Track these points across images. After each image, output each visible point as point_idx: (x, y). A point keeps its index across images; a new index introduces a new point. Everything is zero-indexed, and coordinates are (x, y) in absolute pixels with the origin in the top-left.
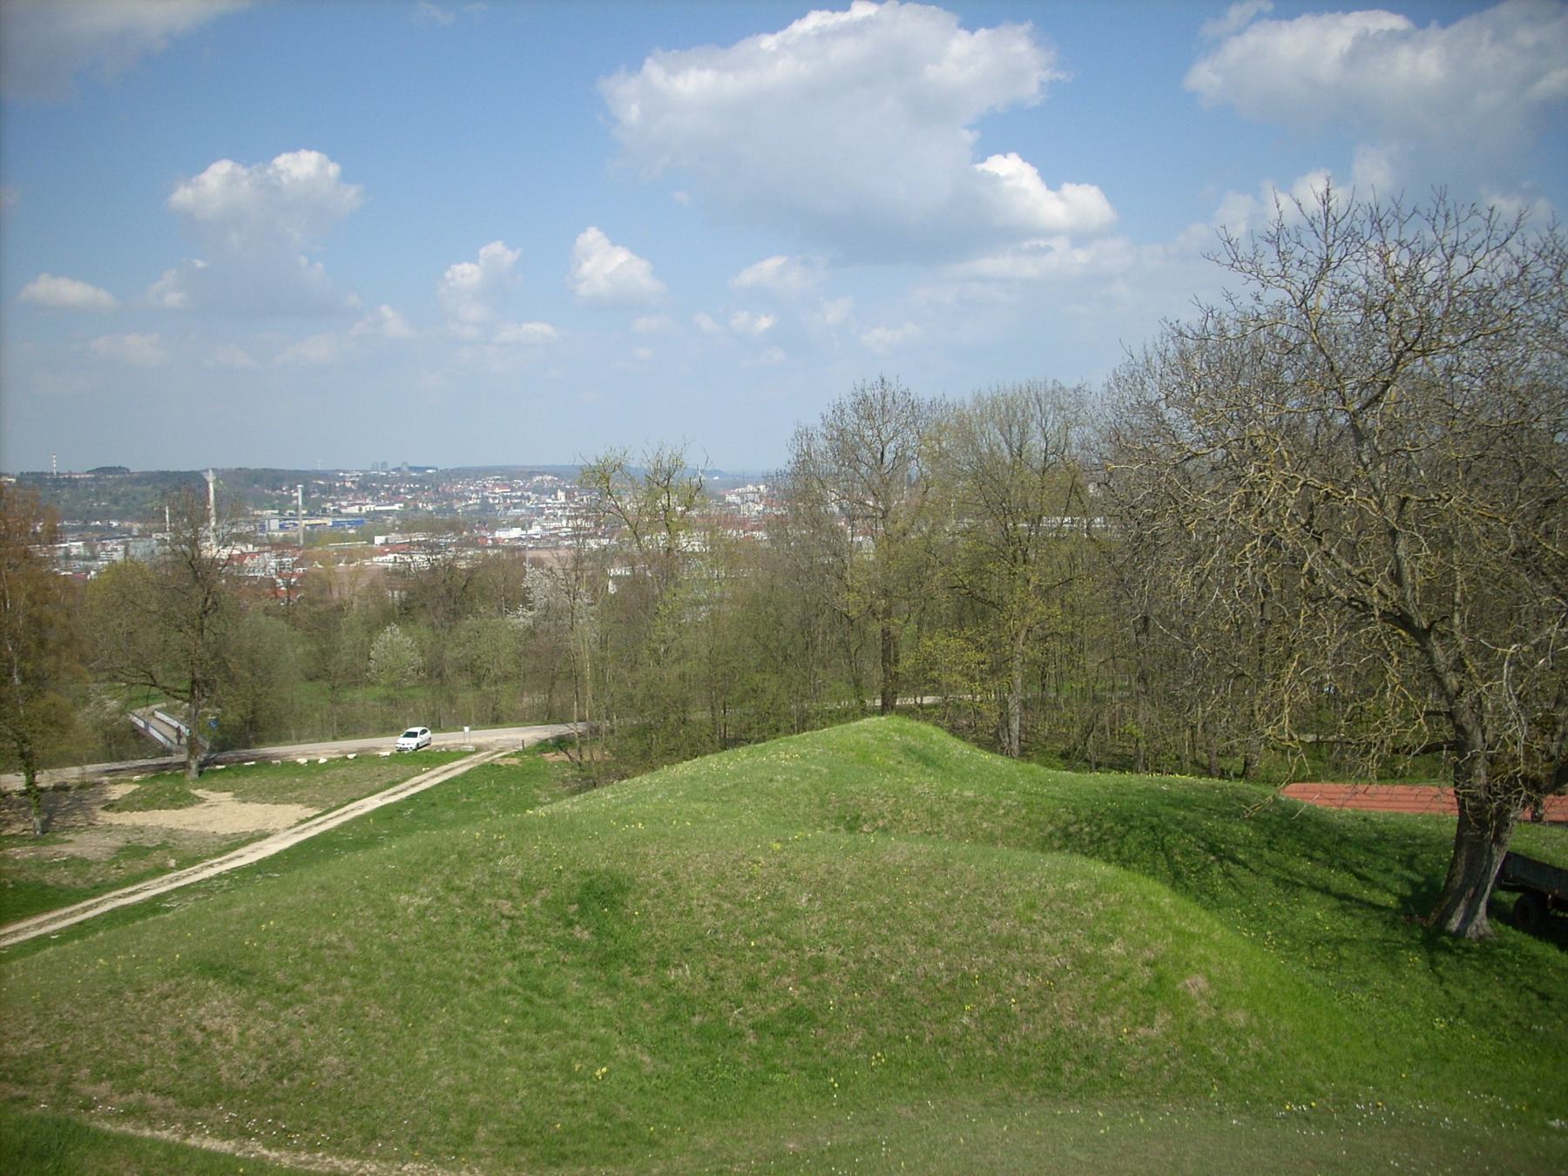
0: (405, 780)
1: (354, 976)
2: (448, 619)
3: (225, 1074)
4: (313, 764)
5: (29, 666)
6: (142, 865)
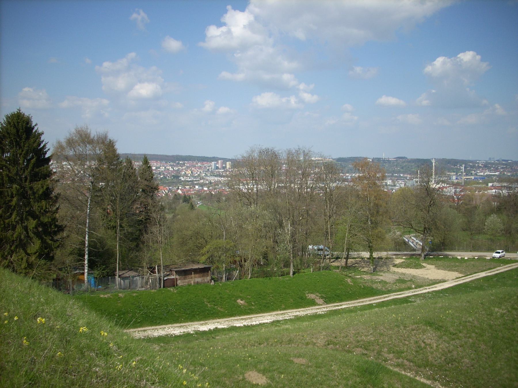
0: (494, 268)
1: (476, 333)
2: (514, 213)
3: (430, 358)
4: (463, 259)
5: (373, 219)
6: (403, 286)
